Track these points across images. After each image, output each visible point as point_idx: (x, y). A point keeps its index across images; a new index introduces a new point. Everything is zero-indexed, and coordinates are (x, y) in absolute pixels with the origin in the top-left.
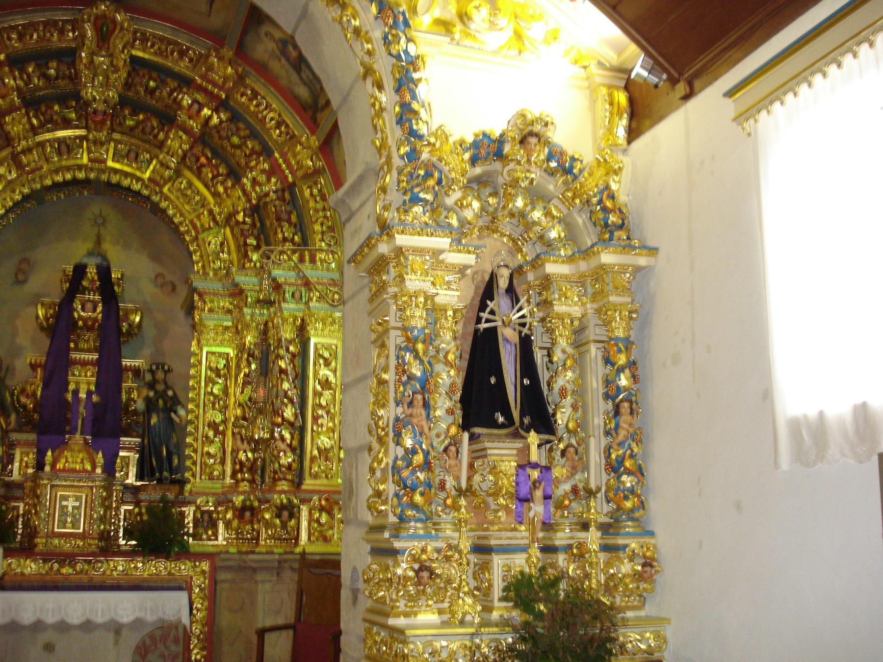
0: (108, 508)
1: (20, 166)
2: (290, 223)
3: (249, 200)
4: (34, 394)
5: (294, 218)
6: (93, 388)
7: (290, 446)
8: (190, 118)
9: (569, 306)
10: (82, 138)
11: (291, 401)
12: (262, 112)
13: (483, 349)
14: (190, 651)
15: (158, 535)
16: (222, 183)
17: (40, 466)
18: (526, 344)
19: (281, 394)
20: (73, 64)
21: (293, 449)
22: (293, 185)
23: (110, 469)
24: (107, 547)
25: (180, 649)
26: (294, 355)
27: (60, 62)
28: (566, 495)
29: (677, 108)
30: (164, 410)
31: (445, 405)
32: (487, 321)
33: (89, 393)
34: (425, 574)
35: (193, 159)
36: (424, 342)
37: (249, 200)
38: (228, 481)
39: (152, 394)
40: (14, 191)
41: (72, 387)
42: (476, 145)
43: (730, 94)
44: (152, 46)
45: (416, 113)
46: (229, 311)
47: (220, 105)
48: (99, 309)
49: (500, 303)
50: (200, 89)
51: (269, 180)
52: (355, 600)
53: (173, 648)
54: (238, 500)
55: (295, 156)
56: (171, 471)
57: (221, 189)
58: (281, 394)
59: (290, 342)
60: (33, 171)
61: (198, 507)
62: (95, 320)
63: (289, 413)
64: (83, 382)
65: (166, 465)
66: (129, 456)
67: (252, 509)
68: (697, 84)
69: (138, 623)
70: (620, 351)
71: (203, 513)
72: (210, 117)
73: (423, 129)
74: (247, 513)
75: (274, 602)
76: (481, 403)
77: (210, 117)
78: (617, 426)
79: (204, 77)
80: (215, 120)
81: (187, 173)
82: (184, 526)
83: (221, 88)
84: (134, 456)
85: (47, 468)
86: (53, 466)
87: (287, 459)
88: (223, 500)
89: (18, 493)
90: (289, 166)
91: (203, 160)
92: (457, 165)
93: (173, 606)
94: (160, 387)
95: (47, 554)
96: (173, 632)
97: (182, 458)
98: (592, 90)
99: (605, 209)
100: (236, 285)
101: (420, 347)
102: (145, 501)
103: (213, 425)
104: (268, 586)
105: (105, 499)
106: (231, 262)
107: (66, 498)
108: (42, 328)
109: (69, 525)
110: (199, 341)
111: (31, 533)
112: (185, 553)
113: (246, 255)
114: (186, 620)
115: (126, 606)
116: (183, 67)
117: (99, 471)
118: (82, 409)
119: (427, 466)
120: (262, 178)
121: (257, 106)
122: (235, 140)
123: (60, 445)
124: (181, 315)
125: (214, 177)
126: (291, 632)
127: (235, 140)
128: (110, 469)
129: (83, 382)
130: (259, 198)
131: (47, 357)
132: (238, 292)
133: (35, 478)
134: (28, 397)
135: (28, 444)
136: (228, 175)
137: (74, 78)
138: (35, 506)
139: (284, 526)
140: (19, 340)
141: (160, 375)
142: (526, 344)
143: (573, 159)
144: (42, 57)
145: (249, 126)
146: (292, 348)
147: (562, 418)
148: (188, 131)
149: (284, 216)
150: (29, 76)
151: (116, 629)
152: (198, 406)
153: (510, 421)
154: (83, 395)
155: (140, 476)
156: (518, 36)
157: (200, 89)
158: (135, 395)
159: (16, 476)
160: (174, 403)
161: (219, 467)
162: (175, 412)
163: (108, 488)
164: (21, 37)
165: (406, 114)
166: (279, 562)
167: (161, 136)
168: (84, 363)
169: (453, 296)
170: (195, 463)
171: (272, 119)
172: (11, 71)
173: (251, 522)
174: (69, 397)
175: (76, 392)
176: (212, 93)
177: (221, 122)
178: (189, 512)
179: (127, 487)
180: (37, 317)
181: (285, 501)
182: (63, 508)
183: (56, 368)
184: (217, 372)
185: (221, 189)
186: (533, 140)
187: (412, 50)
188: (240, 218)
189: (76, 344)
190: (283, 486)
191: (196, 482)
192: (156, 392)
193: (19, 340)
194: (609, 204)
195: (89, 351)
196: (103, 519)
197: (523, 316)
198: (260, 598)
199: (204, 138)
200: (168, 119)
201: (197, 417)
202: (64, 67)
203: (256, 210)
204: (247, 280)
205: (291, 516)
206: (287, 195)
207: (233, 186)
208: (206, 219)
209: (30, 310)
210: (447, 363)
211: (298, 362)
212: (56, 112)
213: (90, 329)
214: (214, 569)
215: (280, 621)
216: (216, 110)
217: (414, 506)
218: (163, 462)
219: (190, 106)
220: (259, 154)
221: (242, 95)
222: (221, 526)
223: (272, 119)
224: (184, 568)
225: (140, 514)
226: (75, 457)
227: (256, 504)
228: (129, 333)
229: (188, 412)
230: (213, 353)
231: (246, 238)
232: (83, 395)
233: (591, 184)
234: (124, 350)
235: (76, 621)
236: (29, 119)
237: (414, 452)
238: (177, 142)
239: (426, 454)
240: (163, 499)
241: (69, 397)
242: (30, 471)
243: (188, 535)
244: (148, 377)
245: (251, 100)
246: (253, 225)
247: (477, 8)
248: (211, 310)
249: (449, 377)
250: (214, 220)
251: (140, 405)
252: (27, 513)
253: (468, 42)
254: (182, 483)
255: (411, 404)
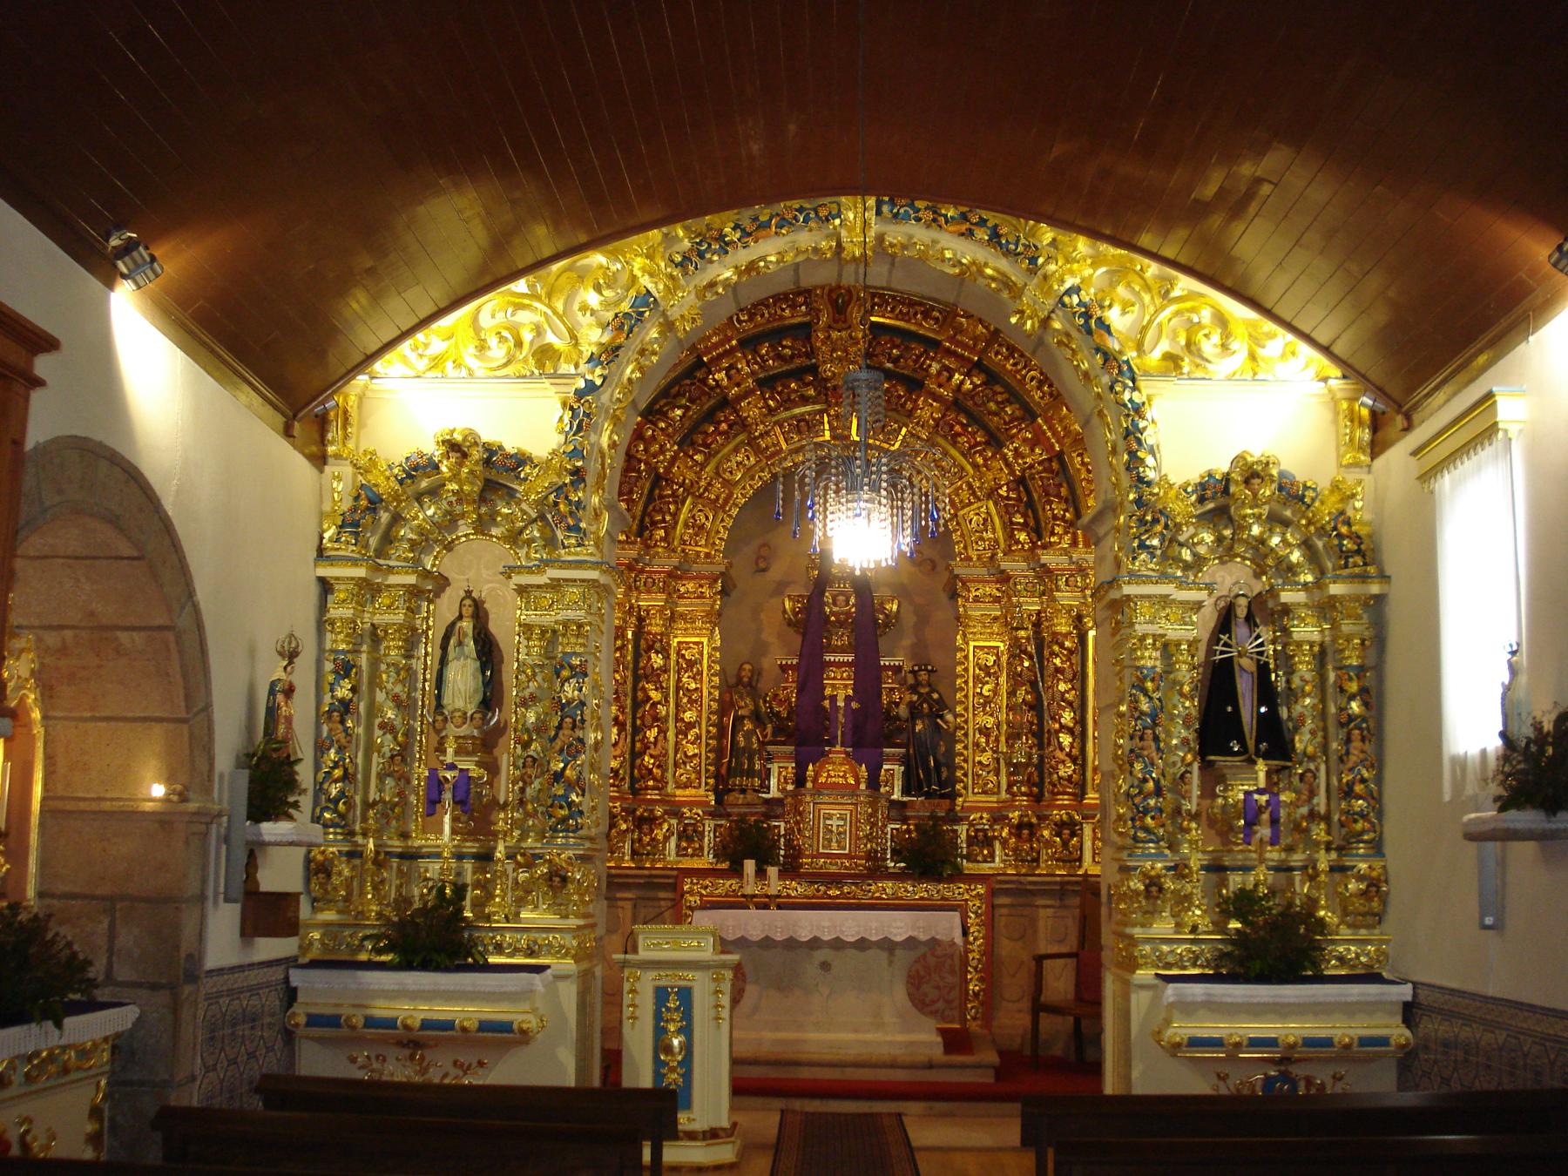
0: (873, 825)
1: (758, 451)
2: (1058, 496)
3: (1012, 472)
4: (788, 699)
5: (1064, 491)
6: (850, 692)
7: (1069, 755)
8: (940, 386)
9: (1307, 631)
10: (821, 412)
11: (1070, 704)
12: (1019, 371)
13: (1218, 679)
14: (967, 982)
15: (928, 857)
16: (980, 453)
17: (800, 781)
18: (1263, 670)
19: (1058, 697)
20: (808, 338)
21: (1074, 760)
22: (1061, 453)
23: (874, 783)
24: (876, 871)
25: (956, 980)
26: (1071, 652)
27: (794, 339)
28: (1303, 817)
29: (1398, 440)
30: (928, 716)
31: (1179, 734)
32: (1222, 653)
33: (848, 699)
34: (1154, 889)
35: (947, 429)
36: (1153, 680)
37: (1012, 472)
38: (1004, 795)
39: (915, 698)
40: (752, 478)
41: (828, 692)
42: (1202, 486)
43: (1414, 453)
44: (893, 310)
45: (1142, 461)
46: (997, 600)
47: (972, 368)
48: (852, 600)
49: (1240, 630)
50: (949, 353)
51: (1032, 450)
52: (1110, 915)
53: (949, 979)
54: (1015, 815)
55: (1061, 421)
56: (942, 785)
57: (980, 460)
58: (1058, 697)
59: (1066, 635)
60: (773, 455)
61: (971, 824)
62: (848, 614)
63: (1067, 717)
64: (839, 687)
65: (934, 775)
66: (893, 770)
67: (1030, 825)
68: (1416, 417)
69: (911, 942)
70: (1350, 679)
71: (977, 831)
72: (962, 382)
73: (1151, 475)
74: (1024, 830)
75: (1052, 928)
76: (1216, 731)
77: (962, 382)
78: (1348, 753)
79: (952, 339)
80: (968, 386)
81: (941, 441)
82: (956, 847)
83: (972, 350)
84: (899, 770)
85: (809, 785)
86: (815, 780)
87: (1066, 770)
88: (998, 817)
89: (779, 811)
90: (1055, 433)
91: (958, 428)
92: (1182, 508)
93: (946, 926)
94: (924, 690)
95: (813, 874)
96: (949, 962)
97: (953, 768)
98: (1335, 402)
99: (1340, 536)
100: (1003, 572)
101: (1149, 685)
102: (914, 817)
103: (985, 731)
104: (1050, 911)
105: (871, 815)
106: (996, 541)
107: (830, 817)
108: (790, 623)
109: (834, 845)
110: (964, 635)
111: (795, 853)
112: (958, 876)
113: (1012, 536)
114: (959, 940)
115: (899, 926)
116: (927, 328)
117: (863, 786)
118: (841, 719)
119: (1158, 792)
120: (1025, 449)
121: (1015, 365)
122: (992, 406)
123: (819, 757)
124: (944, 597)
125: (971, 447)
126: (1071, 962)
127: (992, 406)
128: (874, 783)
129: (839, 687)
130: (1023, 471)
131: (928, 941)
132: (1004, 578)
133: (794, 794)
134: (780, 703)
135: (787, 757)
136: (987, 443)
137: (811, 354)
138: (797, 823)
139: (1065, 844)
140: (764, 636)
141: (923, 676)
142: (1263, 670)
143: (1306, 488)
144: (775, 335)
145: (1008, 388)
146: (1067, 644)
147: (1303, 742)
148: (936, 397)
149: (1052, 490)
150: (762, 357)
151: (888, 945)
152: (966, 709)
153: (1244, 749)
154: (841, 704)
155: (906, 791)
156: (1253, 357)
157: (949, 353)
158: (895, 696)
159: (774, 793)
160: (939, 708)
161: (992, 778)
162: (941, 717)
163: (873, 804)
164: (751, 318)
165: (1135, 462)
166: (1062, 884)
167: (909, 406)
168: (839, 665)
169: (1192, 630)
170: (965, 775)
171: (1032, 379)
172: (745, 356)
173: (1030, 841)
174: (827, 703)
175: (833, 698)
176: (962, 356)
177: (976, 386)
178: (962, 830)
179: (893, 802)
180: (785, 611)
181: (1065, 817)
182: (826, 826)
183: (810, 672)
184: (986, 669)
185: (980, 460)
186: (1257, 481)
187: (1137, 397)
188: (1003, 491)
189: (830, 641)
190: (1065, 800)
191: (969, 797)
192: (920, 695)
193: (764, 636)
194: (1344, 530)
195: (842, 650)
196: (869, 838)
197: (1261, 645)
198: (1041, 924)
199: (958, 404)
200: (915, 385)
201: (966, 722)
202: (799, 345)
203: (1021, 482)
204: (1015, 566)
205: (1073, 834)
206: (1055, 465)
207: (994, 456)
208: (965, 495)
209: (775, 601)
210: (1182, 694)
211: (1075, 659)
212: (794, 391)
213: (841, 624)
214: (992, 893)
215: (1064, 950)
216: (968, 374)
217: (1147, 829)
218: (932, 774)
219: (939, 373)
220: (1022, 419)
221: (997, 354)
222: (997, 845)
223: (1032, 379)
224: (958, 891)
225: (908, 831)
226: (837, 769)
227: (1034, 820)
228: (886, 625)
229: (956, 716)
230: (982, 648)
231: (1011, 515)
232: (841, 704)
233: (1325, 512)
234: (883, 643)
235: (850, 939)
236: (765, 400)
237: (1145, 780)
238: (928, 411)
239: (1157, 782)
240: (933, 817)
241: (827, 703)
242: (790, 787)
243: (963, 857)
244: (911, 680)
245: (1007, 359)
246: (1019, 499)
247: (1206, 335)
248: (977, 599)
249: (1187, 705)
250: (974, 493)
251: (903, 711)
252: (789, 831)
253: (1199, 374)
254: (953, 796)
255: (1142, 739)
